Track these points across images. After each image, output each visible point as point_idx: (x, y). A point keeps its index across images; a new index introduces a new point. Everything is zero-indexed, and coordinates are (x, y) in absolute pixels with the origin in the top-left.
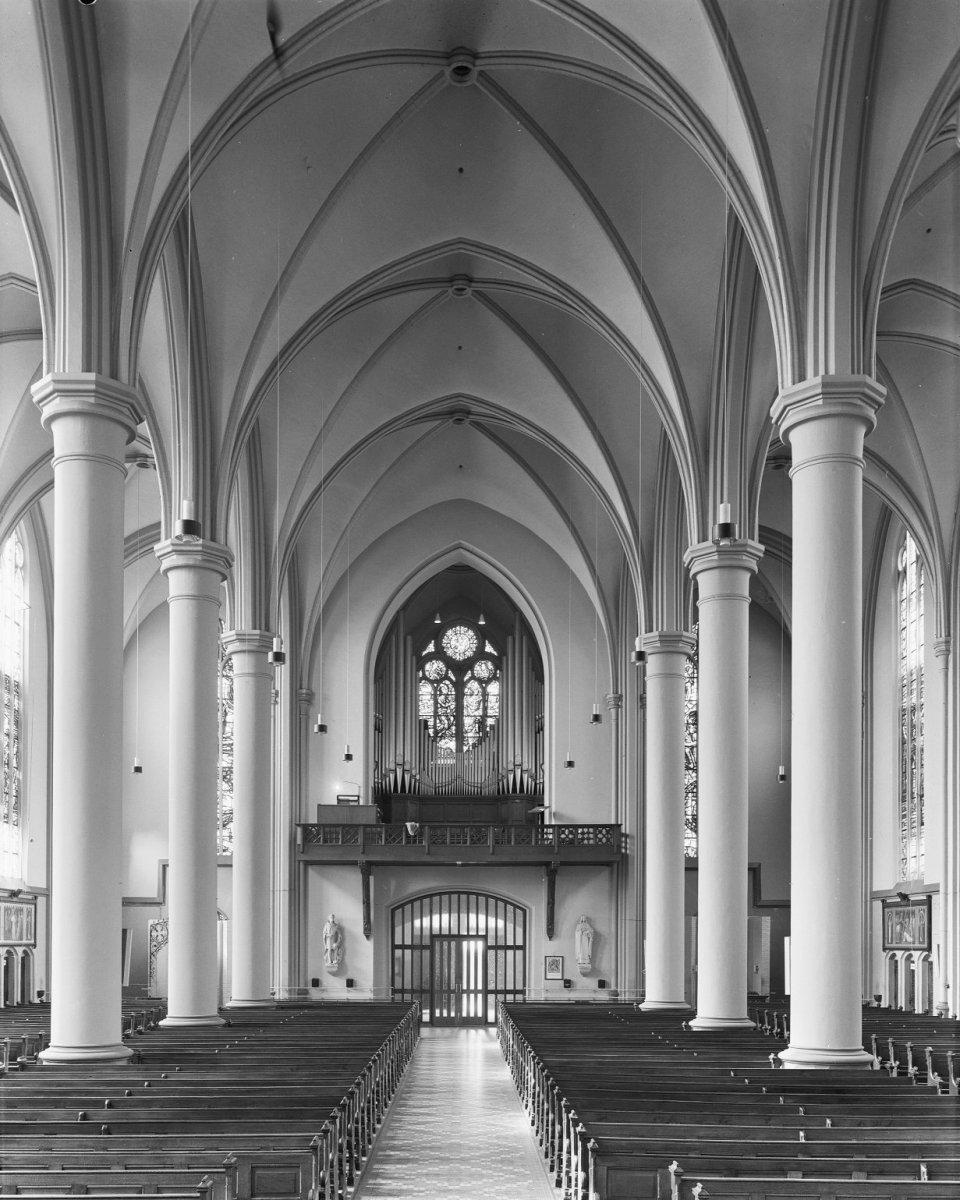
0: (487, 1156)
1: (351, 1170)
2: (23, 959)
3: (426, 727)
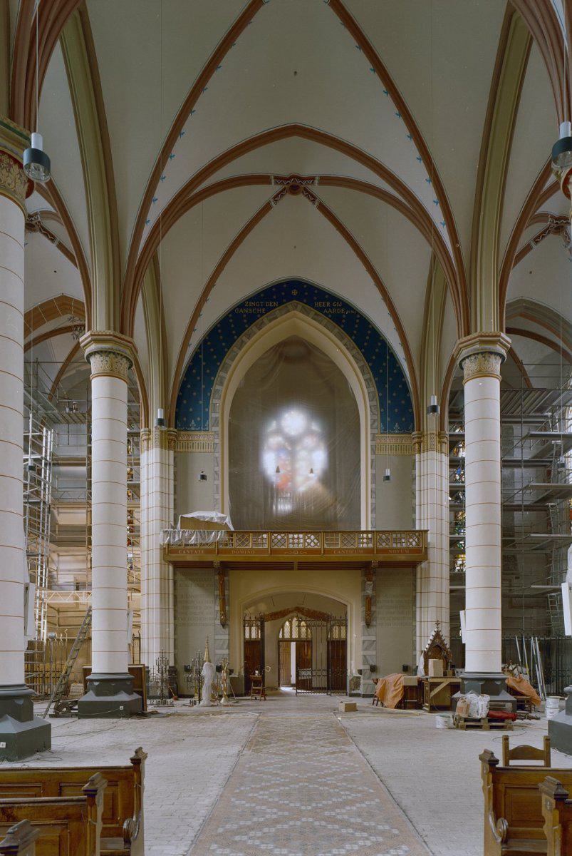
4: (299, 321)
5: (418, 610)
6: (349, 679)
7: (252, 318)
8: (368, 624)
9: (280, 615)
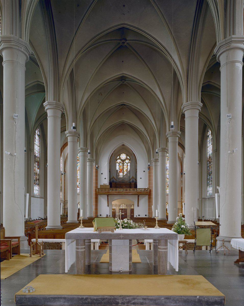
3: (118, 171)
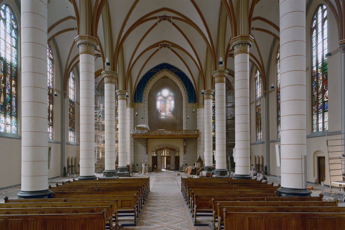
0: (172, 198)
1: (143, 201)
2: (71, 159)
4: (166, 74)
5: (198, 149)
6: (180, 167)
7: (154, 73)
8: (185, 153)
9: (162, 149)
